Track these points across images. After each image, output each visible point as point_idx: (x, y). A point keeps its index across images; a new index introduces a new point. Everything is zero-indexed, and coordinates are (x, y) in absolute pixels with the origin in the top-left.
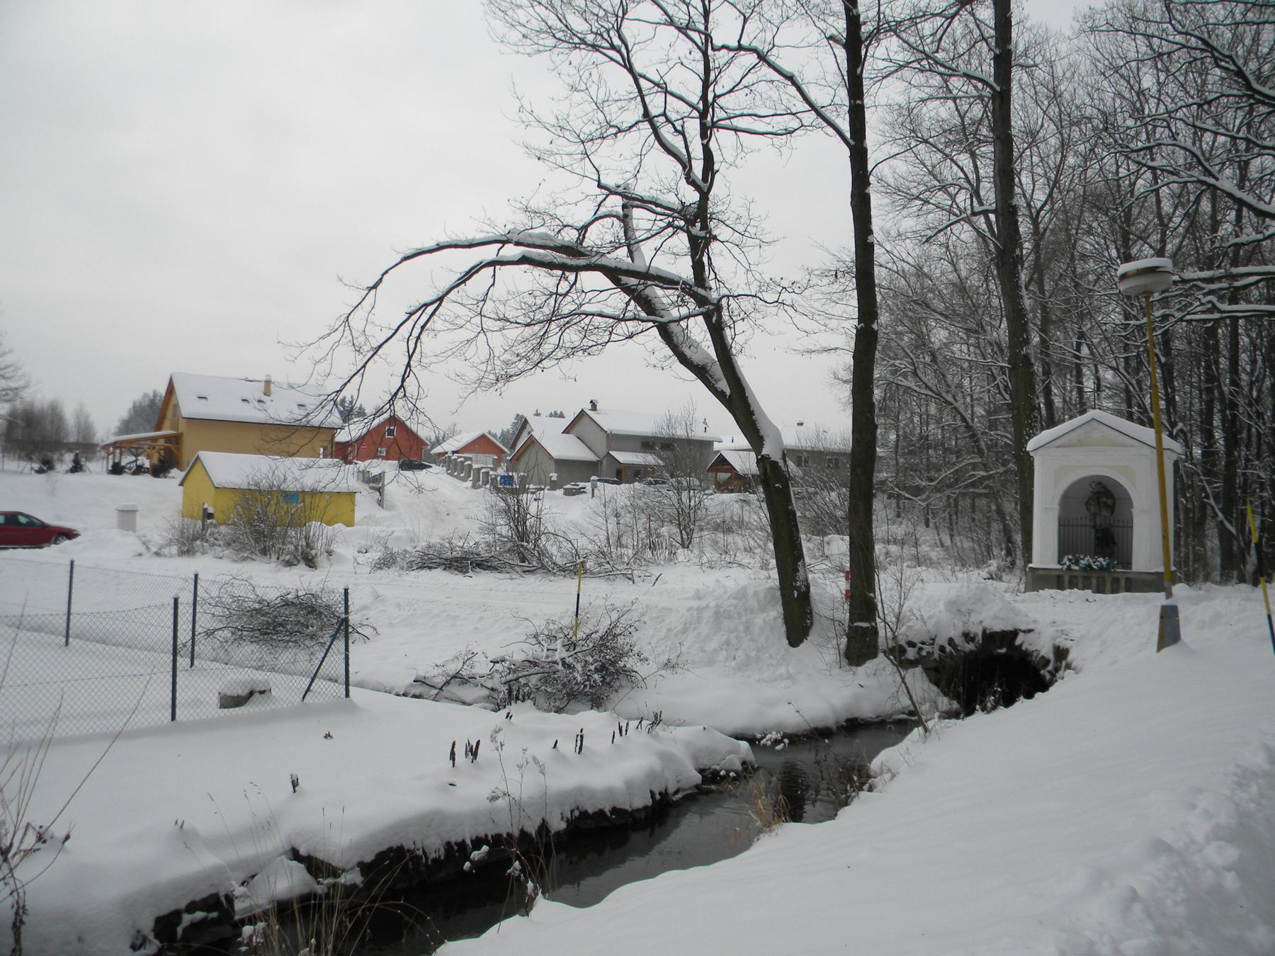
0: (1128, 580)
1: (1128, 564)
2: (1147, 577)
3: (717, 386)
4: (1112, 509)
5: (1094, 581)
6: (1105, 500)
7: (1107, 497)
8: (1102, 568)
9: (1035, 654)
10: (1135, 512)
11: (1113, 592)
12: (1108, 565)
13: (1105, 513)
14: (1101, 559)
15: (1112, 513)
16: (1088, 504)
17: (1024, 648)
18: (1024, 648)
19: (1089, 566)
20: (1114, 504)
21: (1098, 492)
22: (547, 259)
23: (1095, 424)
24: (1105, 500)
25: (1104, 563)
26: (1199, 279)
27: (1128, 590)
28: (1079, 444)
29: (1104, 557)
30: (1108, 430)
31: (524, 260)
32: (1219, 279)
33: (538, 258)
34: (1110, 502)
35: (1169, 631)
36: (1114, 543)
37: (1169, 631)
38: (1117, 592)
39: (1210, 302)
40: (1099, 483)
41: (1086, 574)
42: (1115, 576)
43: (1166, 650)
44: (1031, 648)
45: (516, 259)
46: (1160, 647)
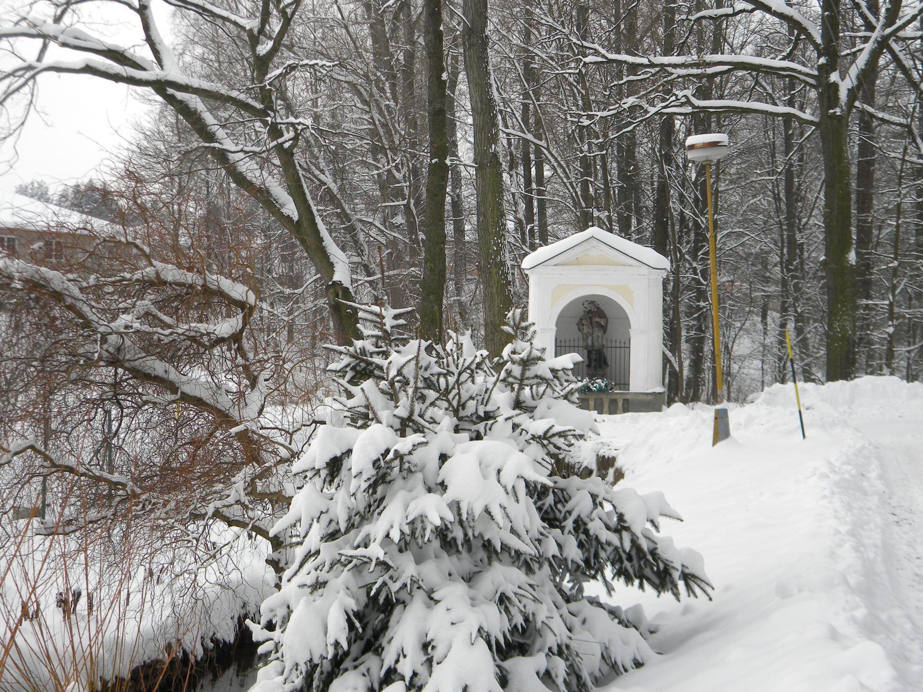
0: (626, 401)
1: (626, 385)
2: (645, 397)
3: (283, 210)
4: (604, 329)
5: (592, 403)
6: (598, 320)
7: (600, 317)
8: (600, 390)
9: (577, 466)
10: (632, 333)
11: (610, 413)
12: (606, 386)
13: (598, 333)
14: (599, 381)
15: (605, 333)
16: (580, 324)
17: (566, 461)
18: (566, 461)
19: (588, 388)
20: (607, 323)
21: (590, 312)
22: (112, 71)
23: (594, 242)
24: (598, 320)
25: (603, 385)
26: (669, 65)
27: (626, 410)
28: (577, 262)
29: (602, 378)
30: (607, 248)
31: (89, 69)
32: (692, 65)
33: (103, 69)
34: (603, 322)
35: (721, 431)
36: (605, 363)
37: (721, 431)
38: (616, 413)
39: (685, 96)
40: (592, 303)
41: (583, 396)
42: (613, 397)
43: (720, 444)
44: (572, 461)
45: (78, 67)
46: (715, 442)
